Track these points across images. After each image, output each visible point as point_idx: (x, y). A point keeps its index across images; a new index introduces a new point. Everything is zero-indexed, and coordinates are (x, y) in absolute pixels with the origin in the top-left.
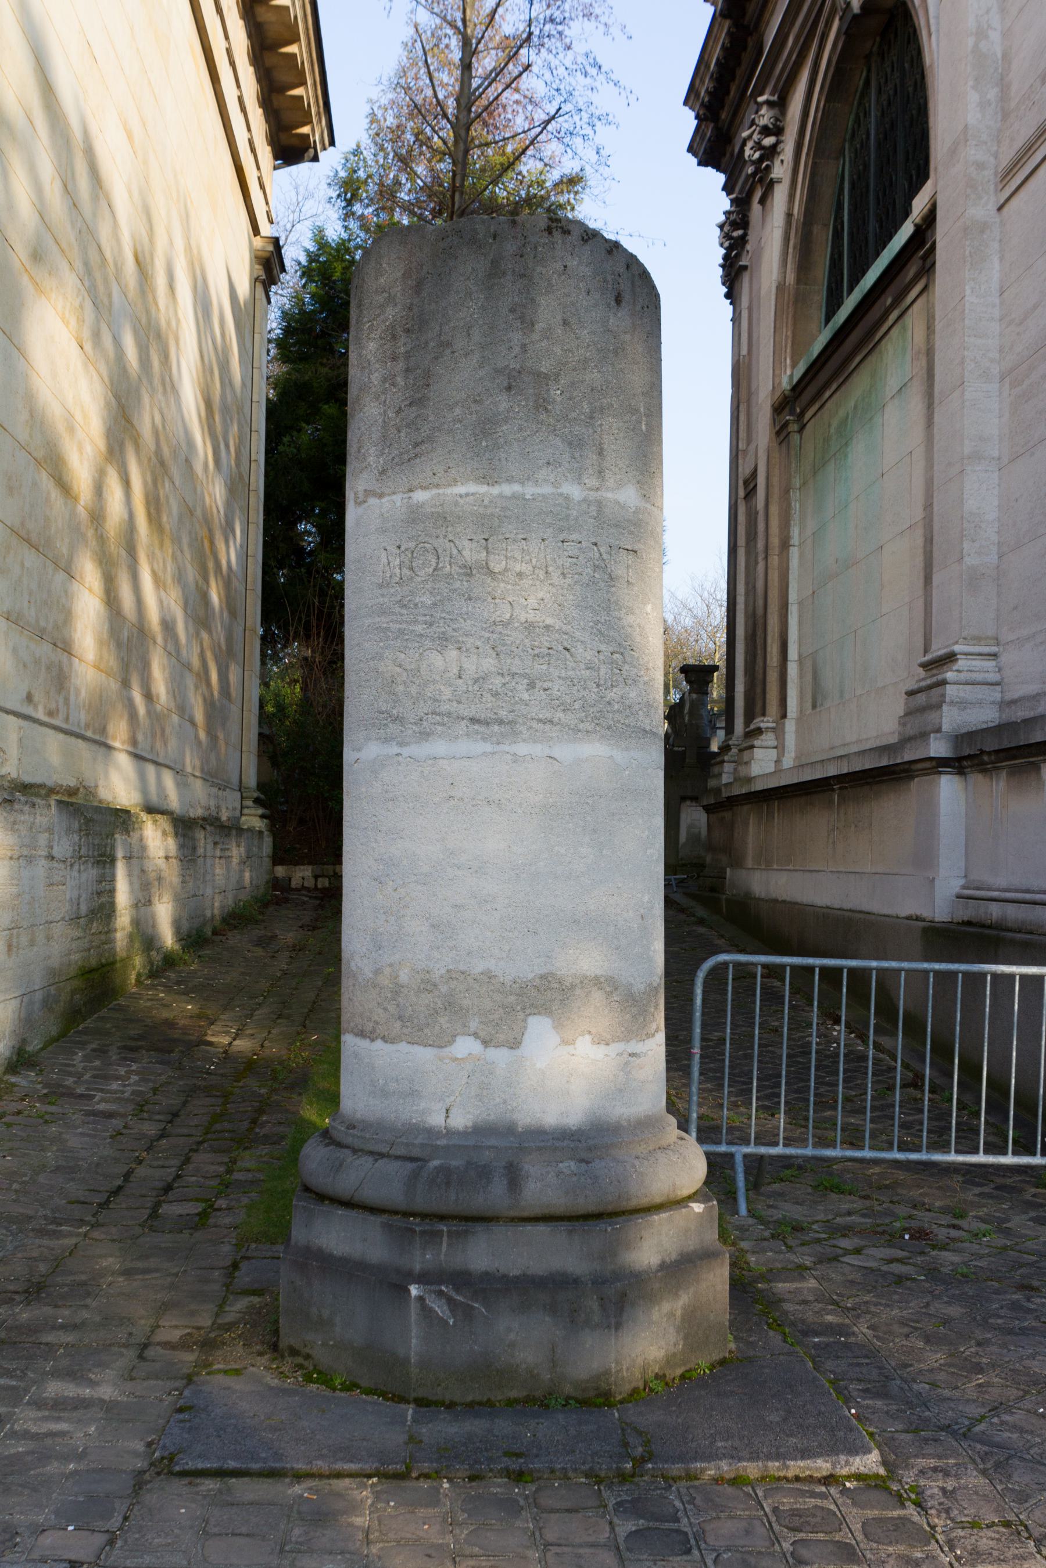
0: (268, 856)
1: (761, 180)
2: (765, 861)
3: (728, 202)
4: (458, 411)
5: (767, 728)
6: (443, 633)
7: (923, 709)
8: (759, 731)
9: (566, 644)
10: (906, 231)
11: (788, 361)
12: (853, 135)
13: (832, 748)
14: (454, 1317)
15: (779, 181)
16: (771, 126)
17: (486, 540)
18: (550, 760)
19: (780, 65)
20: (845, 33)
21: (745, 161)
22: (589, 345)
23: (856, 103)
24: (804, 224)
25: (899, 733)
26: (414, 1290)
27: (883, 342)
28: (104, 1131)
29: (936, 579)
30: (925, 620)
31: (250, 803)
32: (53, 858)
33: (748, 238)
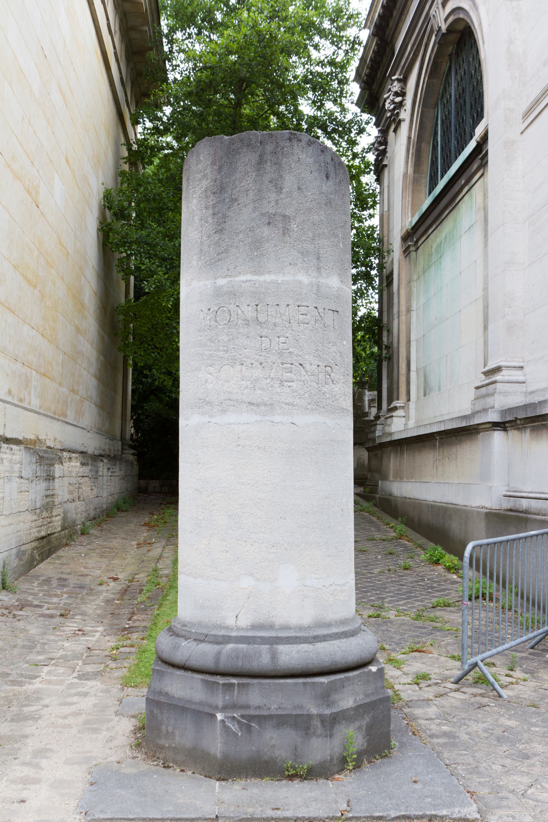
0: (136, 475)
1: (394, 119)
2: (399, 476)
3: (377, 132)
4: (241, 236)
5: (400, 407)
6: (234, 356)
7: (484, 396)
8: (395, 408)
9: (300, 362)
10: (472, 145)
11: (409, 214)
12: (443, 96)
13: (435, 417)
14: (241, 732)
15: (404, 120)
16: (399, 92)
17: (257, 305)
18: (292, 425)
19: (404, 60)
20: (438, 43)
21: (386, 110)
22: (312, 201)
23: (444, 79)
24: (417, 142)
25: (472, 409)
26: (220, 716)
27: (460, 203)
28: (49, 625)
29: (490, 327)
30: (484, 349)
31: (126, 447)
32: (22, 478)
33: (387, 150)
